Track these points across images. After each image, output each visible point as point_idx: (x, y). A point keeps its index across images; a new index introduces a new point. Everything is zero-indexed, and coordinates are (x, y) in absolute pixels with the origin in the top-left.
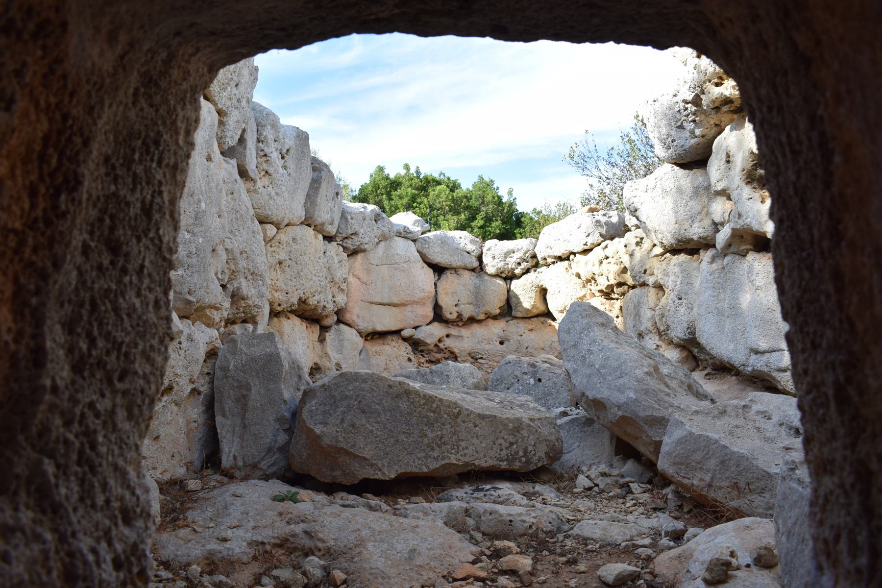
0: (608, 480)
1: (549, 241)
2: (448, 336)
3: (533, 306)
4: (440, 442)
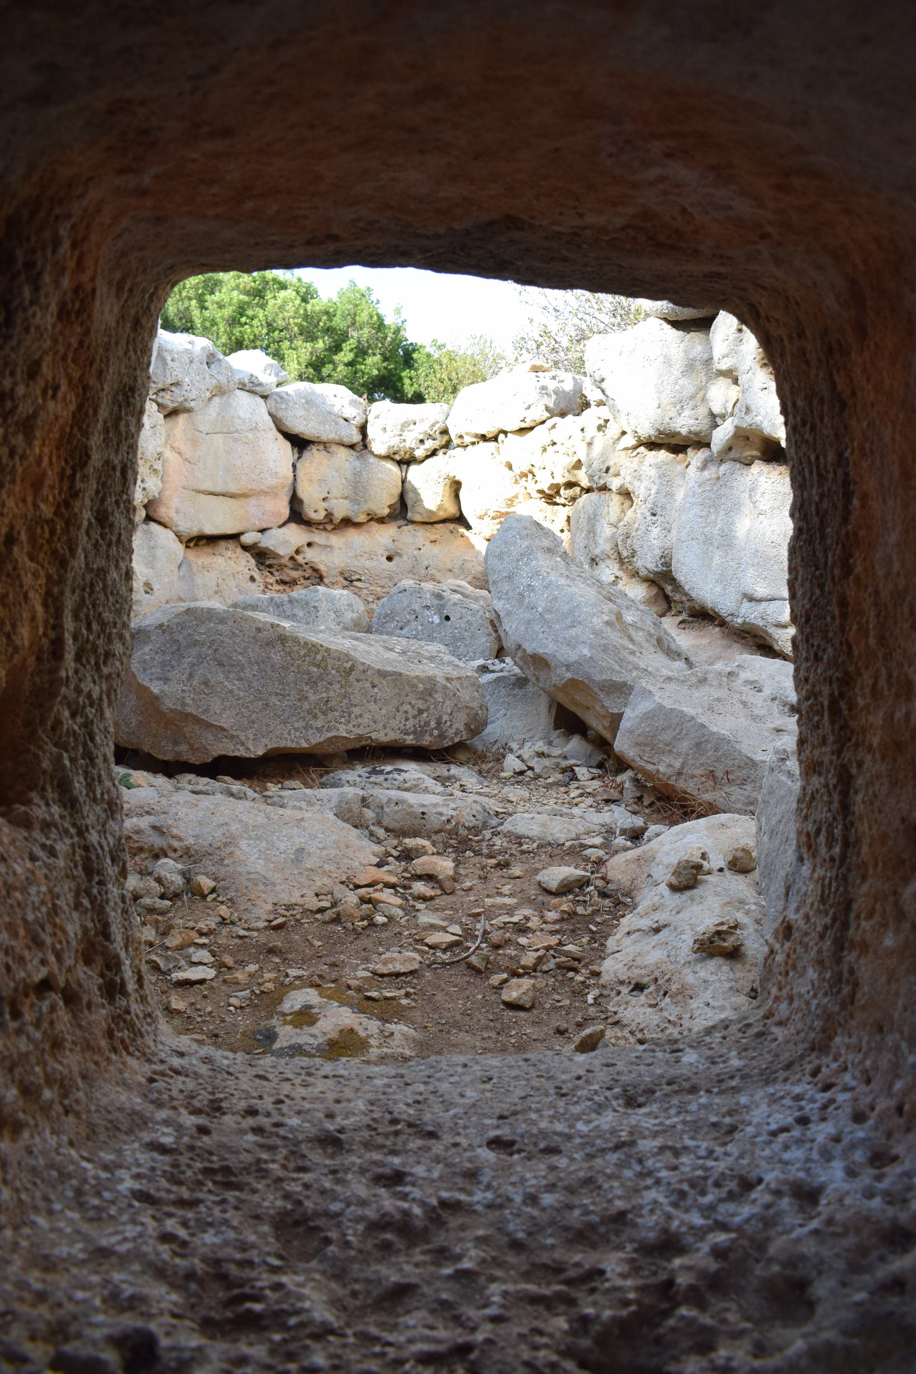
0: (546, 762)
1: (467, 412)
2: (309, 545)
3: (440, 507)
4: (326, 707)
